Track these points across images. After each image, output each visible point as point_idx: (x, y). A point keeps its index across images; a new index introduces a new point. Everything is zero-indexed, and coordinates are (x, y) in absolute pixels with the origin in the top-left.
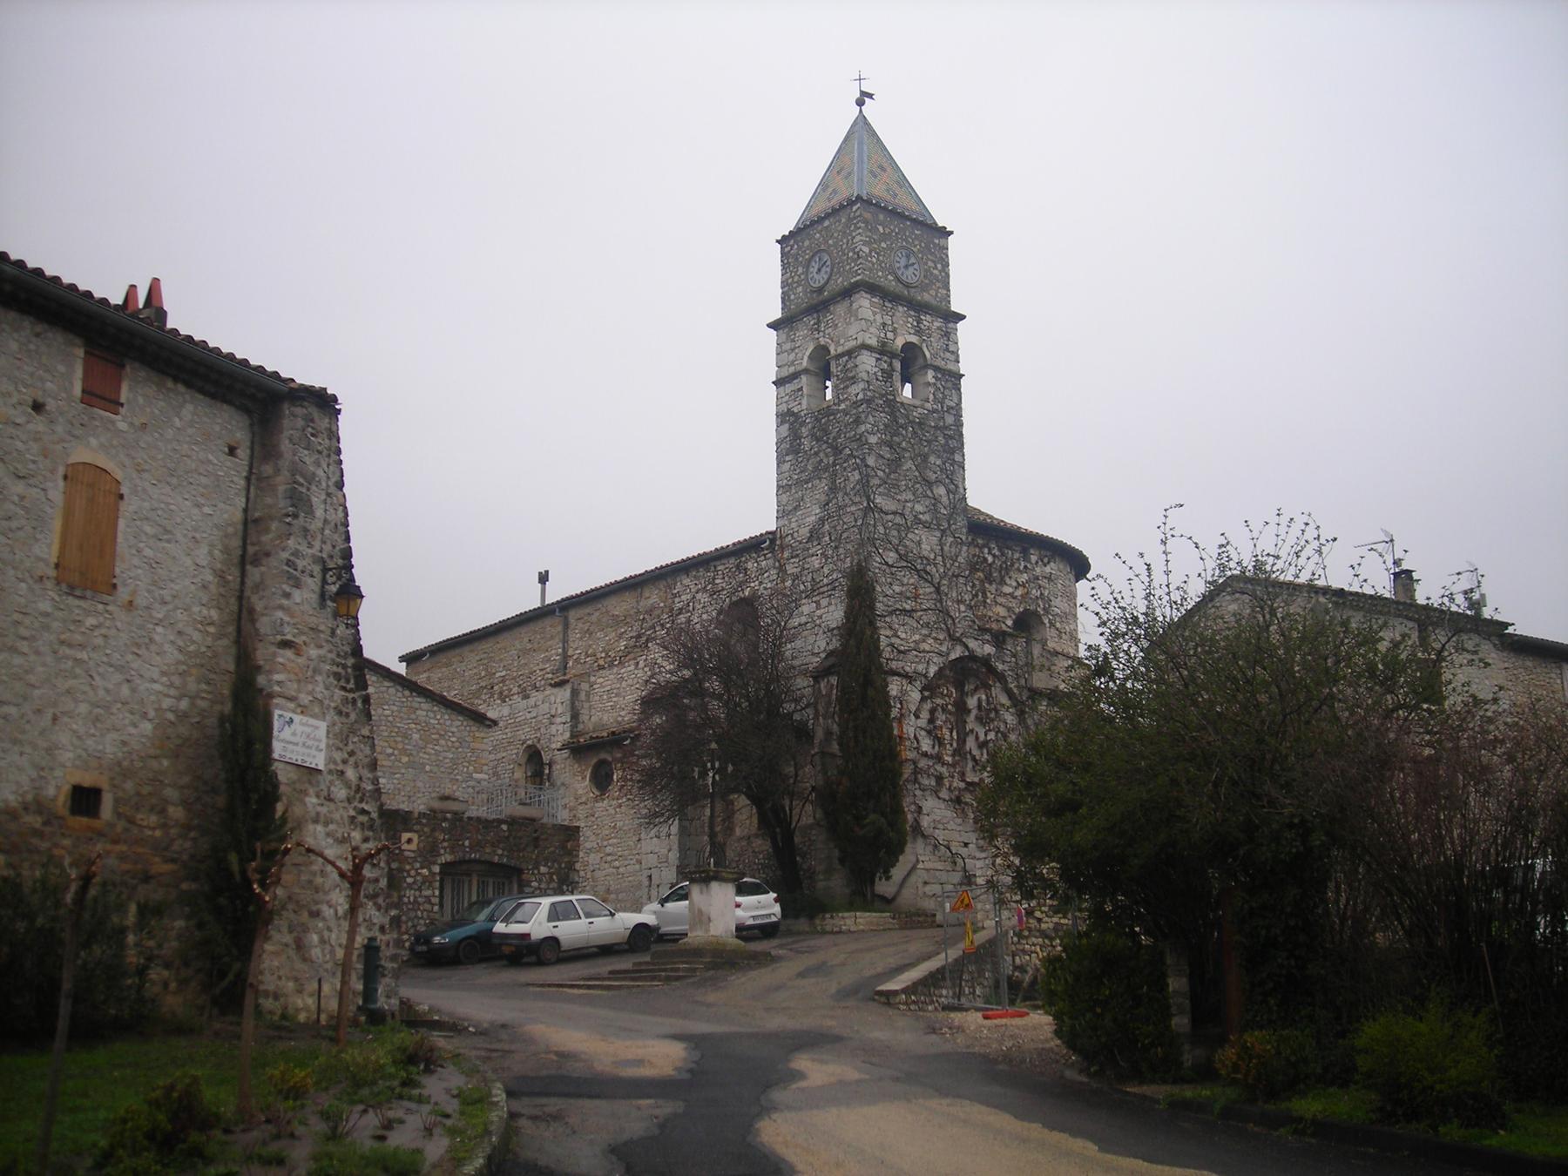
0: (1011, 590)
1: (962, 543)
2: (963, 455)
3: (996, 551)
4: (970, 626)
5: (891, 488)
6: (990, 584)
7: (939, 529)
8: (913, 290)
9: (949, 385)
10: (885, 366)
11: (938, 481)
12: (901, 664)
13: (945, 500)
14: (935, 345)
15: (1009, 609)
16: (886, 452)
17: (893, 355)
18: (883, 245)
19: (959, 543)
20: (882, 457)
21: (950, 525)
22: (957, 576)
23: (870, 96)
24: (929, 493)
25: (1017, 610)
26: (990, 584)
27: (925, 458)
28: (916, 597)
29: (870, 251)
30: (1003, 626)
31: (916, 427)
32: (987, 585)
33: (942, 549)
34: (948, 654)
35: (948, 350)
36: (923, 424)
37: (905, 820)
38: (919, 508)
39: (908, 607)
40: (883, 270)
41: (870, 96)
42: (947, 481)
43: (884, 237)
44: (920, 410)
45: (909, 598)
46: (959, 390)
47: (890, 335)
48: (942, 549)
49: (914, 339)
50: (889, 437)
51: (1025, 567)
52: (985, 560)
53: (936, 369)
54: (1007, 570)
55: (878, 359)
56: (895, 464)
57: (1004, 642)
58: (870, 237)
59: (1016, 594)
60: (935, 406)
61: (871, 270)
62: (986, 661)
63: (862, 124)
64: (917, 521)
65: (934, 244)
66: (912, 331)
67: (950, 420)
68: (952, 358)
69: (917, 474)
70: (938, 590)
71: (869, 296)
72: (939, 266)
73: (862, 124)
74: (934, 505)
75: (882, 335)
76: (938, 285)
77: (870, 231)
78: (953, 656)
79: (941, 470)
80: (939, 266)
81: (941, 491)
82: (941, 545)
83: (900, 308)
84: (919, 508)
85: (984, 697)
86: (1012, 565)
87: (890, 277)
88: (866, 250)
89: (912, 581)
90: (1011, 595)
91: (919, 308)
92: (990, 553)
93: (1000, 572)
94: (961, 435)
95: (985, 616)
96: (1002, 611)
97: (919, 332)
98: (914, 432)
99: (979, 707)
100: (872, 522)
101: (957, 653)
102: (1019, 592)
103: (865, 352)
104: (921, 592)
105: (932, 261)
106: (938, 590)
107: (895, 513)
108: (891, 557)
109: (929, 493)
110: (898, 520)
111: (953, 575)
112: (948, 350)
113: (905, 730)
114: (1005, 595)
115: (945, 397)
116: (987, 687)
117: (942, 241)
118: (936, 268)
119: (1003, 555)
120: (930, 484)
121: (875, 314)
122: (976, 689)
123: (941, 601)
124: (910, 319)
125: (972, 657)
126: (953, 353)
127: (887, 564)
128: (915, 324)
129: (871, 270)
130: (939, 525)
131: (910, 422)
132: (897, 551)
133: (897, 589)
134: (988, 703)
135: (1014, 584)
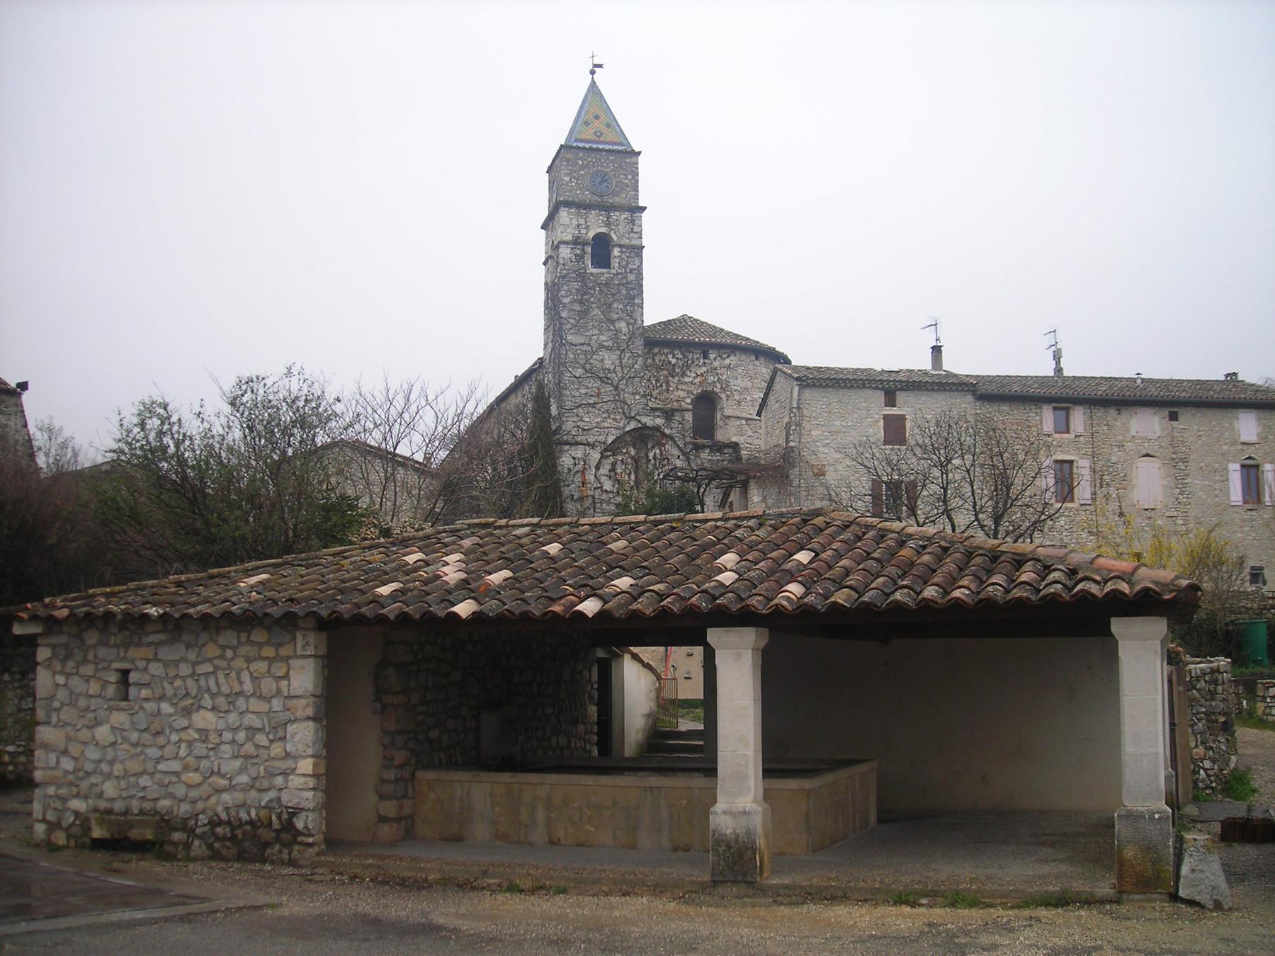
0: (691, 379)
1: (639, 356)
2: (642, 299)
3: (680, 356)
4: (644, 409)
5: (579, 328)
6: (673, 377)
7: (619, 350)
8: (606, 197)
9: (633, 254)
10: (579, 252)
11: (619, 319)
12: (584, 437)
13: (625, 330)
14: (621, 230)
15: (688, 392)
16: (577, 307)
17: (584, 244)
18: (582, 172)
19: (635, 356)
20: (574, 310)
21: (628, 346)
22: (633, 378)
23: (600, 66)
24: (612, 327)
25: (695, 392)
26: (673, 377)
27: (610, 306)
28: (599, 394)
29: (571, 180)
30: (683, 404)
31: (602, 287)
32: (670, 378)
33: (621, 362)
34: (624, 428)
35: (632, 232)
36: (610, 284)
37: (1027, 598)
38: (603, 338)
39: (592, 402)
40: (580, 189)
41: (600, 66)
42: (628, 318)
43: (583, 167)
44: (606, 275)
45: (592, 396)
46: (641, 256)
47: (583, 231)
48: (621, 362)
49: (603, 230)
50: (580, 297)
51: (704, 363)
52: (670, 362)
53: (620, 246)
54: (688, 367)
55: (572, 249)
56: (584, 314)
57: (673, 415)
58: (570, 170)
59: (695, 381)
60: (619, 271)
61: (570, 191)
62: (657, 429)
63: (593, 87)
64: (601, 346)
65: (626, 163)
66: (602, 225)
67: (631, 277)
68: (637, 236)
69: (602, 317)
70: (616, 388)
71: (567, 209)
72: (630, 177)
73: (593, 87)
74: (615, 335)
75: (577, 232)
76: (628, 189)
77: (571, 165)
78: (628, 429)
79: (623, 311)
80: (630, 177)
81: (622, 325)
82: (620, 358)
83: (593, 212)
84: (603, 338)
85: (658, 451)
86: (693, 362)
87: (587, 193)
88: (567, 179)
89: (596, 385)
90: (692, 383)
91: (608, 209)
92: (674, 357)
93: (682, 368)
94: (641, 286)
95: (668, 399)
96: (682, 394)
97: (608, 224)
98: (601, 291)
99: (655, 458)
100: (564, 352)
101: (633, 425)
102: (697, 380)
103: (562, 246)
104: (603, 391)
105: (623, 174)
106: (616, 388)
107: (583, 344)
108: (579, 372)
109: (612, 327)
110: (585, 348)
111: (630, 377)
112: (632, 232)
113: (587, 478)
114: (686, 383)
115: (628, 263)
116: (660, 445)
117: (633, 160)
118: (627, 178)
119: (684, 357)
120: (613, 322)
121: (571, 219)
122: (653, 447)
123: (618, 395)
124: (601, 218)
125: (645, 427)
126: (637, 233)
127: (575, 376)
128: (605, 219)
129: (570, 191)
130: (619, 347)
131: (598, 284)
132: (584, 368)
133: (583, 391)
134: (661, 454)
135: (695, 375)
